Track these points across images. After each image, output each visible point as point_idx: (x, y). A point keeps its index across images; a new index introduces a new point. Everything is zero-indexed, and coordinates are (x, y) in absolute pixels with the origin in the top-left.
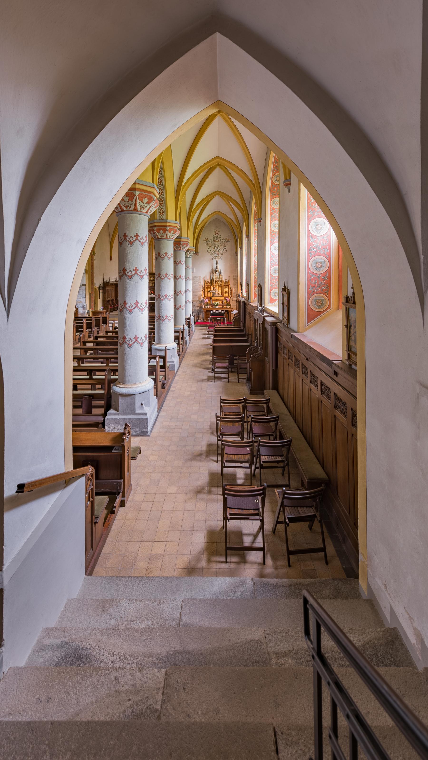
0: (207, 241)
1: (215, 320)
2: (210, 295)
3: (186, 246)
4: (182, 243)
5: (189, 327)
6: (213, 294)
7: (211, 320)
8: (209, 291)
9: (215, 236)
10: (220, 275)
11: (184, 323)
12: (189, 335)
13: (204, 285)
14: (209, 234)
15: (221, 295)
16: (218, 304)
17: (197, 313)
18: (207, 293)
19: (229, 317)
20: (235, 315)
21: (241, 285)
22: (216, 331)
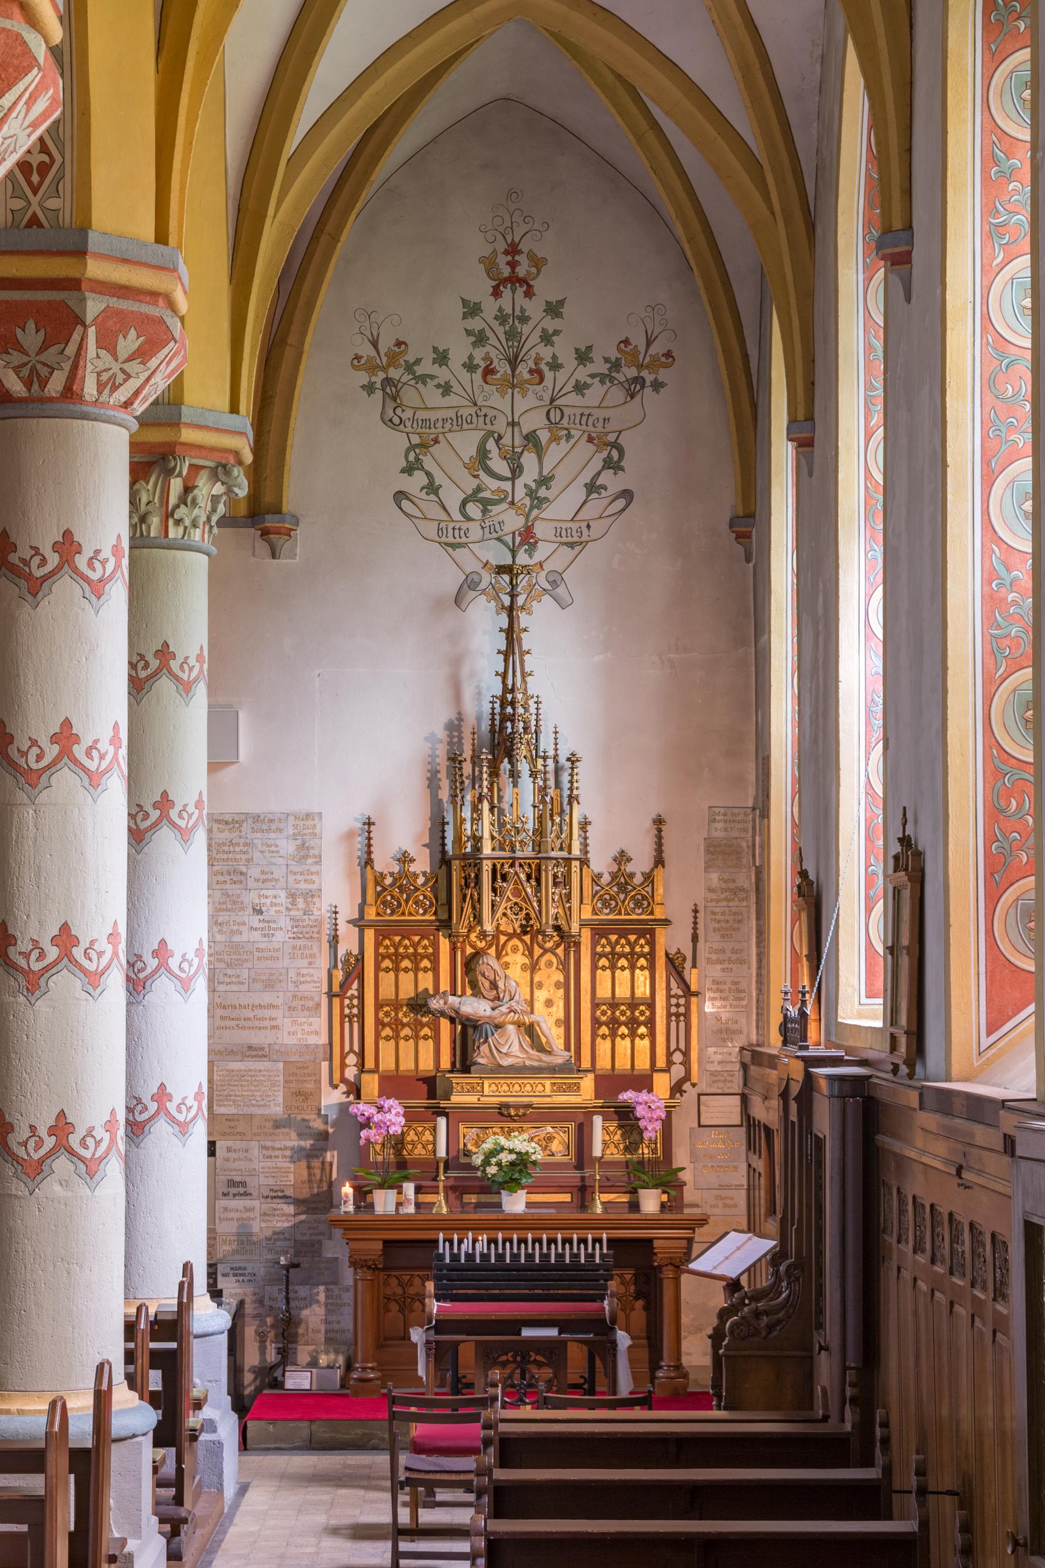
0: (390, 375)
1: (488, 1356)
2: (426, 1055)
3: (143, 354)
4: (94, 306)
5: (168, 1434)
6: (469, 1033)
7: (442, 1354)
8: (418, 1005)
9: (490, 307)
10: (556, 805)
11: (113, 1348)
12: (174, 1527)
13: (360, 923)
14: (413, 290)
15: (560, 1056)
16: (522, 1162)
17: (269, 1281)
18: (390, 1026)
19: (655, 1341)
20: (733, 1286)
21: (814, 900)
22: (512, 1450)
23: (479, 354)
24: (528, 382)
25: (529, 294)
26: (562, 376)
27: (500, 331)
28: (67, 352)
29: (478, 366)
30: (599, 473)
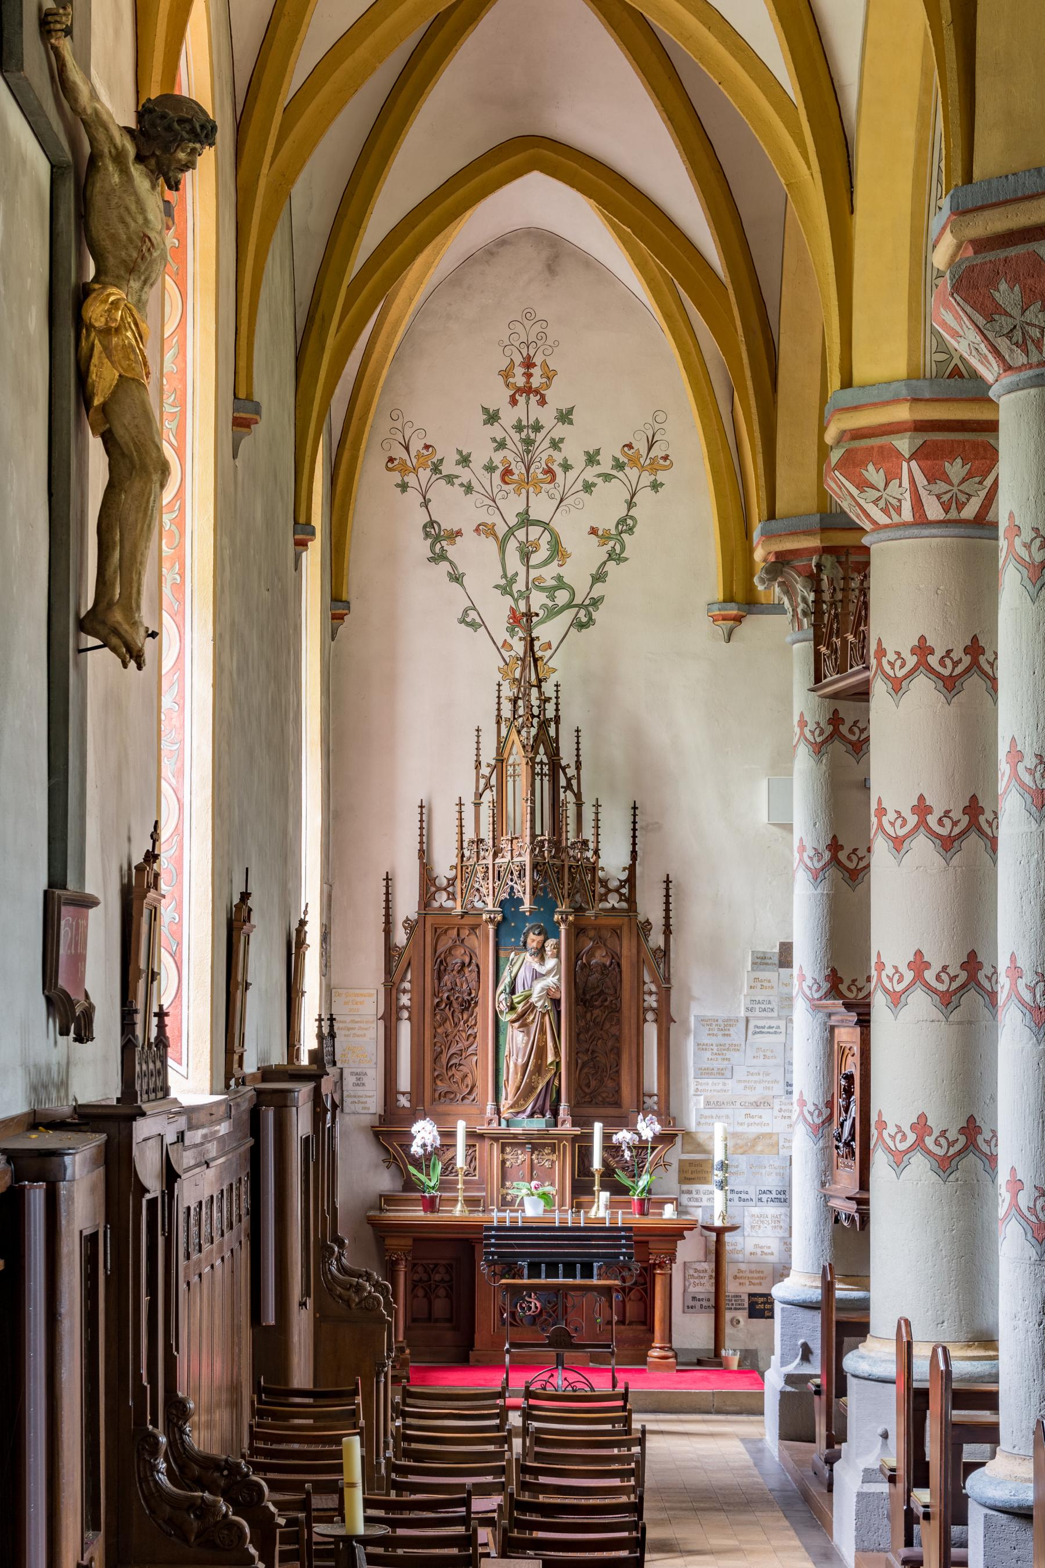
23: (498, 458)
24: (542, 481)
25: (543, 402)
26: (572, 475)
27: (516, 437)
28: (985, 483)
29: (497, 467)
30: (605, 563)
